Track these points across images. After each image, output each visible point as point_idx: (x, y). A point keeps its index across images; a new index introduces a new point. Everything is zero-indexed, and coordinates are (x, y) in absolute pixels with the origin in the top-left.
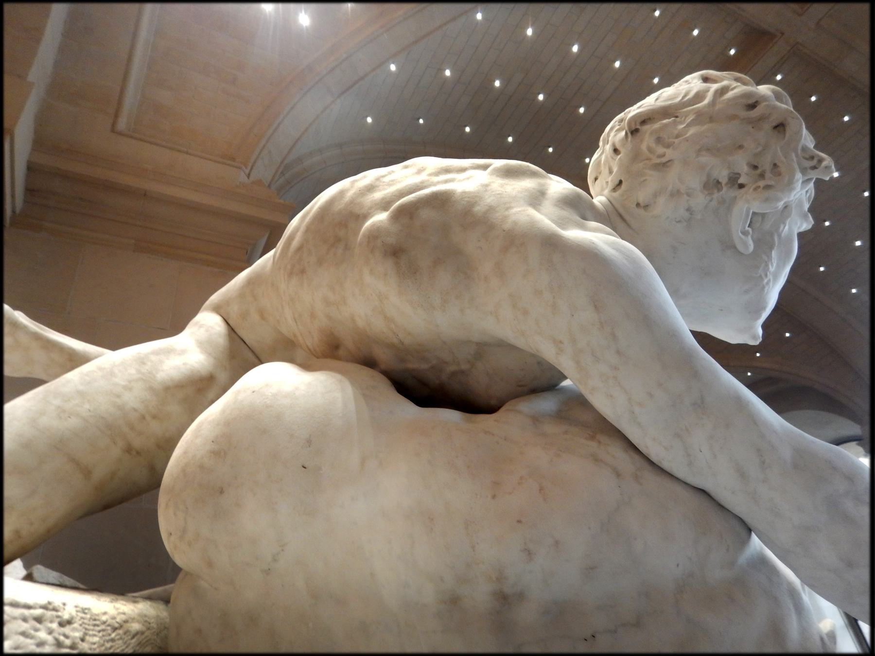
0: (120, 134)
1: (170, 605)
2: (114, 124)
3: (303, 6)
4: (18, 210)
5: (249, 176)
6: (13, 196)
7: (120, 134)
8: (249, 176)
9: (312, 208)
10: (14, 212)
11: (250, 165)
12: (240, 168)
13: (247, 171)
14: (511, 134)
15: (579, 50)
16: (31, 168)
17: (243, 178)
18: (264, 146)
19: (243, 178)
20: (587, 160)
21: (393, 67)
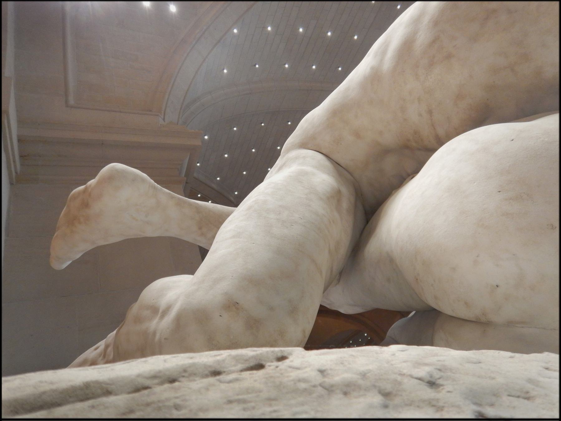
0: (72, 107)
1: (263, 363)
2: (67, 102)
3: (172, 2)
4: (19, 172)
5: (164, 120)
6: (14, 161)
7: (72, 107)
8: (164, 120)
9: (386, 45)
10: (16, 173)
11: (163, 112)
12: (157, 115)
13: (162, 117)
14: (314, 64)
15: (400, 8)
16: (20, 140)
17: (161, 122)
18: (168, 99)
19: (161, 122)
20: (269, 169)
21: (235, 31)
